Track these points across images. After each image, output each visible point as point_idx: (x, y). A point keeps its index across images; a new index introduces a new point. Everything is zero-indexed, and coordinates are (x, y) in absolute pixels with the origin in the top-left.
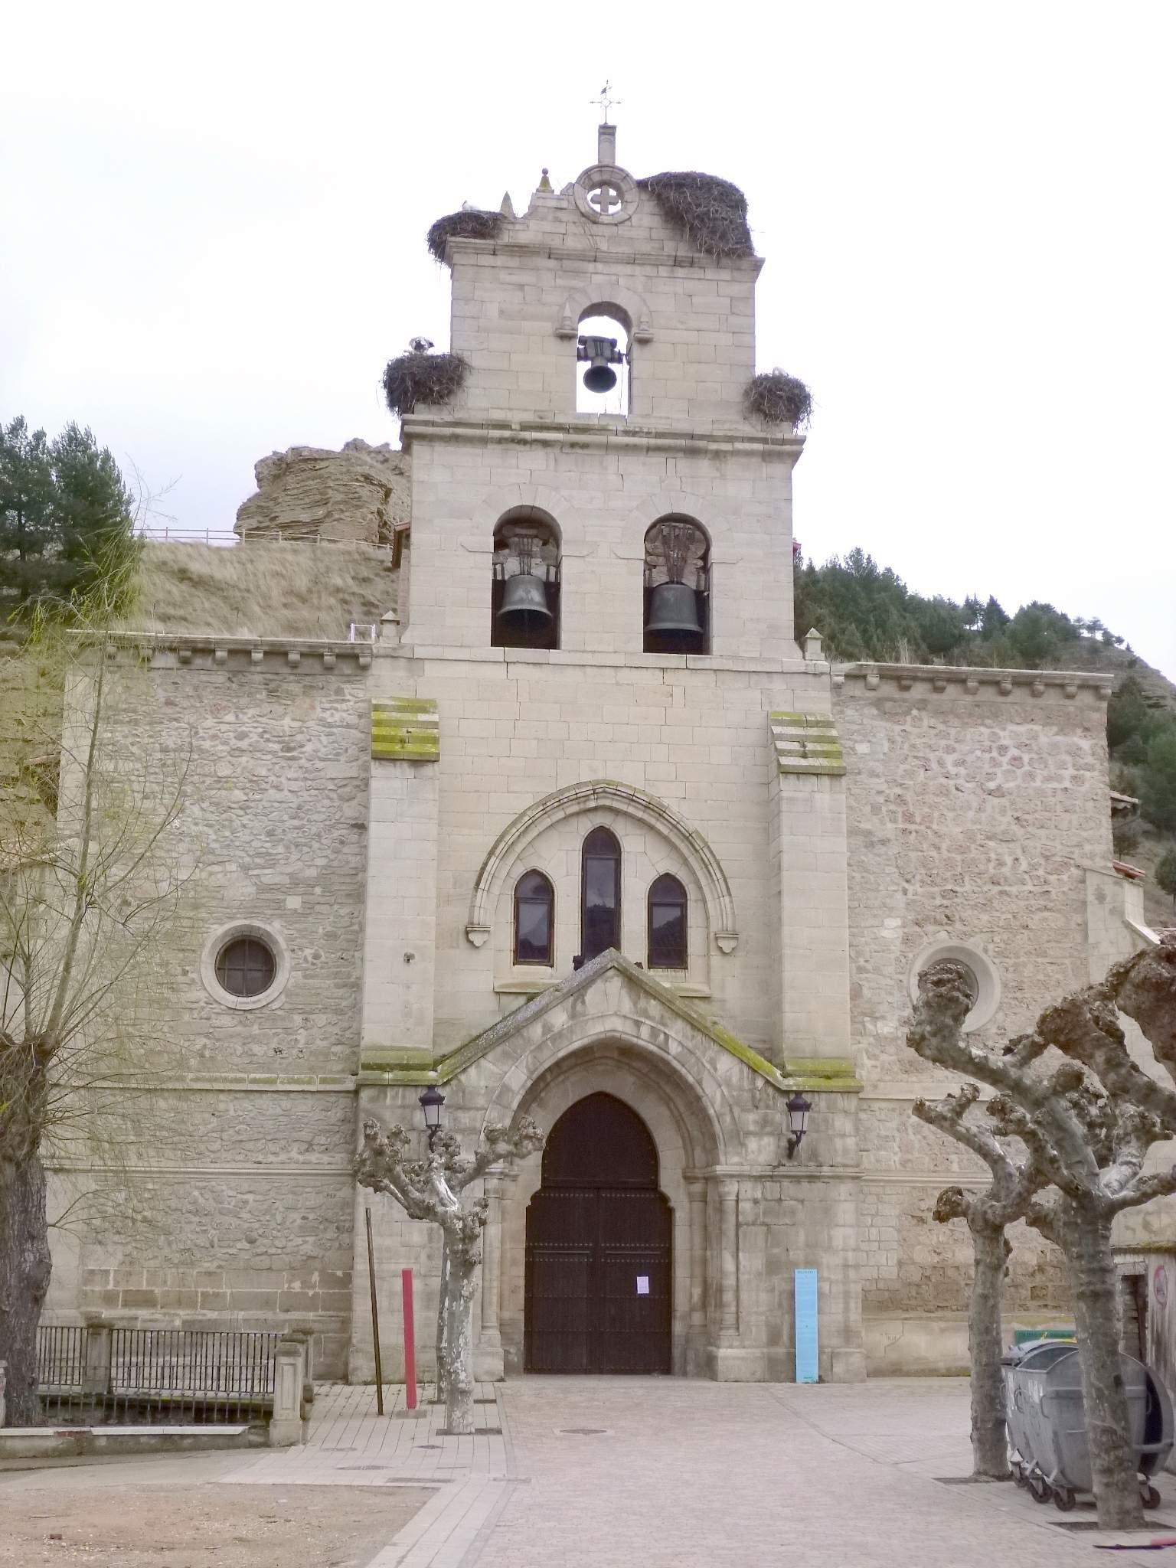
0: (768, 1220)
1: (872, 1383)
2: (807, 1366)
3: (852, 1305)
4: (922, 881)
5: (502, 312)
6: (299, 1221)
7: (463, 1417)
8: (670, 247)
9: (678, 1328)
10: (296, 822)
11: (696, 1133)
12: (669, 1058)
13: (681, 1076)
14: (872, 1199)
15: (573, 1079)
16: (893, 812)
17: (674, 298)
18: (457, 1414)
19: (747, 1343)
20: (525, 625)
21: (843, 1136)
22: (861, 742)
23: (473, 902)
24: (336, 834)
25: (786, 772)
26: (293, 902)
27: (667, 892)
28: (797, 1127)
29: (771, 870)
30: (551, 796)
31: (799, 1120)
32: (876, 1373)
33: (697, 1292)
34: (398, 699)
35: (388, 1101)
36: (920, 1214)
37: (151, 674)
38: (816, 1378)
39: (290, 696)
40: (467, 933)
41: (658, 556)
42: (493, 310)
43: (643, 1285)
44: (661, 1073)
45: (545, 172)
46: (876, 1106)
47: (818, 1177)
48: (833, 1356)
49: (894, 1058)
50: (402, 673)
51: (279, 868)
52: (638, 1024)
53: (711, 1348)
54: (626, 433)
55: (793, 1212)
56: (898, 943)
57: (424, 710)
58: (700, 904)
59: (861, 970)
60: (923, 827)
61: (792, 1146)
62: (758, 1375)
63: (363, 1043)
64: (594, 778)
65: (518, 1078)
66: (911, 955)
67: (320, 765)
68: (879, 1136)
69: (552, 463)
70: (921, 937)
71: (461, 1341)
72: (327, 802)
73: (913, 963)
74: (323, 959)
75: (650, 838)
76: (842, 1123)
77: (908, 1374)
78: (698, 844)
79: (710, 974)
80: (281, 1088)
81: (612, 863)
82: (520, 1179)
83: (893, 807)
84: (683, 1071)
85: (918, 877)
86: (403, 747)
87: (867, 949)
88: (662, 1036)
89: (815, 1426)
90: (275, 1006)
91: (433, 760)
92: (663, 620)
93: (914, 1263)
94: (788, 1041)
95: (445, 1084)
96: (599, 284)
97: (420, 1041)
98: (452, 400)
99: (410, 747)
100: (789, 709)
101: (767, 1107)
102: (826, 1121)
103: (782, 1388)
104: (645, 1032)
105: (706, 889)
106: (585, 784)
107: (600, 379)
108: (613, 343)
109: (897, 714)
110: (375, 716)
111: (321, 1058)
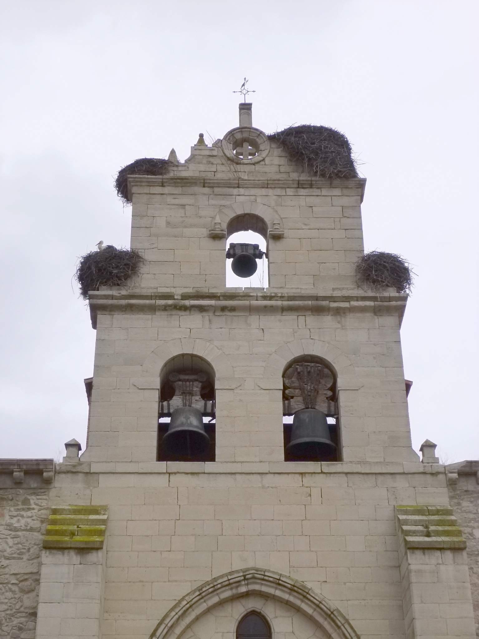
5: (168, 223)
8: (295, 176)
17: (299, 209)
24: (16, 622)
25: (413, 548)
30: (207, 583)
41: (295, 388)
42: (161, 222)
45: (201, 136)
64: (243, 566)
69: (207, 322)
72: (9, 595)
78: (340, 621)
91: (98, 548)
96: (242, 203)
98: (129, 282)
106: (237, 571)
108: (256, 247)
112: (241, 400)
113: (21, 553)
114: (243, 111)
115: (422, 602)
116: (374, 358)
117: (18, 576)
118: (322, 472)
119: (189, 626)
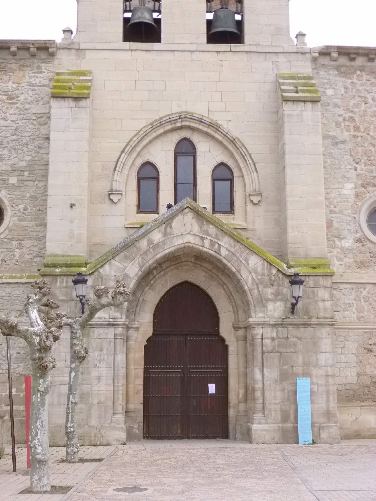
0: (280, 350)
1: (345, 444)
2: (305, 435)
3: (331, 398)
4: (365, 163)
6: (15, 355)
7: (40, 480)
9: (232, 412)
10: (15, 137)
11: (239, 302)
12: (221, 258)
13: (229, 269)
14: (342, 338)
15: (170, 274)
16: (348, 126)
18: (36, 477)
19: (269, 421)
21: (324, 301)
22: (329, 88)
23: (113, 178)
24: (36, 143)
26: (13, 180)
27: (223, 175)
28: (296, 294)
29: (279, 156)
30: (156, 121)
31: (298, 290)
32: (346, 437)
33: (242, 392)
34: (69, 70)
35: (58, 284)
36: (369, 347)
38: (311, 441)
39: (13, 71)
43: (212, 389)
44: (218, 269)
46: (342, 286)
47: (310, 325)
48: (320, 428)
49: (352, 260)
51: (4, 162)
52: (203, 239)
53: (250, 424)
55: (295, 345)
56: (353, 196)
58: (241, 179)
59: (332, 212)
60: (365, 134)
61: (293, 306)
62: (276, 440)
63: (47, 253)
65: (133, 271)
66: (360, 204)
67: (28, 106)
68: (344, 303)
70: (366, 193)
71: (38, 424)
72: (31, 126)
73: (361, 208)
74: (29, 210)
75: (212, 144)
76: (323, 294)
77: (364, 438)
78: (239, 144)
79: (249, 217)
80: (5, 281)
81: (192, 158)
82: (141, 329)
83: (347, 123)
84: (229, 265)
85: (363, 161)
87: (335, 200)
88: (217, 246)
89: (305, 482)
92: (217, 28)
93: (366, 374)
94: (291, 248)
95: (90, 274)
97: (80, 251)
99: (73, 91)
101: (279, 285)
102: (313, 292)
103: (288, 448)
104: (207, 243)
105: (243, 170)
106: (175, 113)
109: (348, 73)
111: (28, 265)
117: (37, 115)
119: (145, 147)
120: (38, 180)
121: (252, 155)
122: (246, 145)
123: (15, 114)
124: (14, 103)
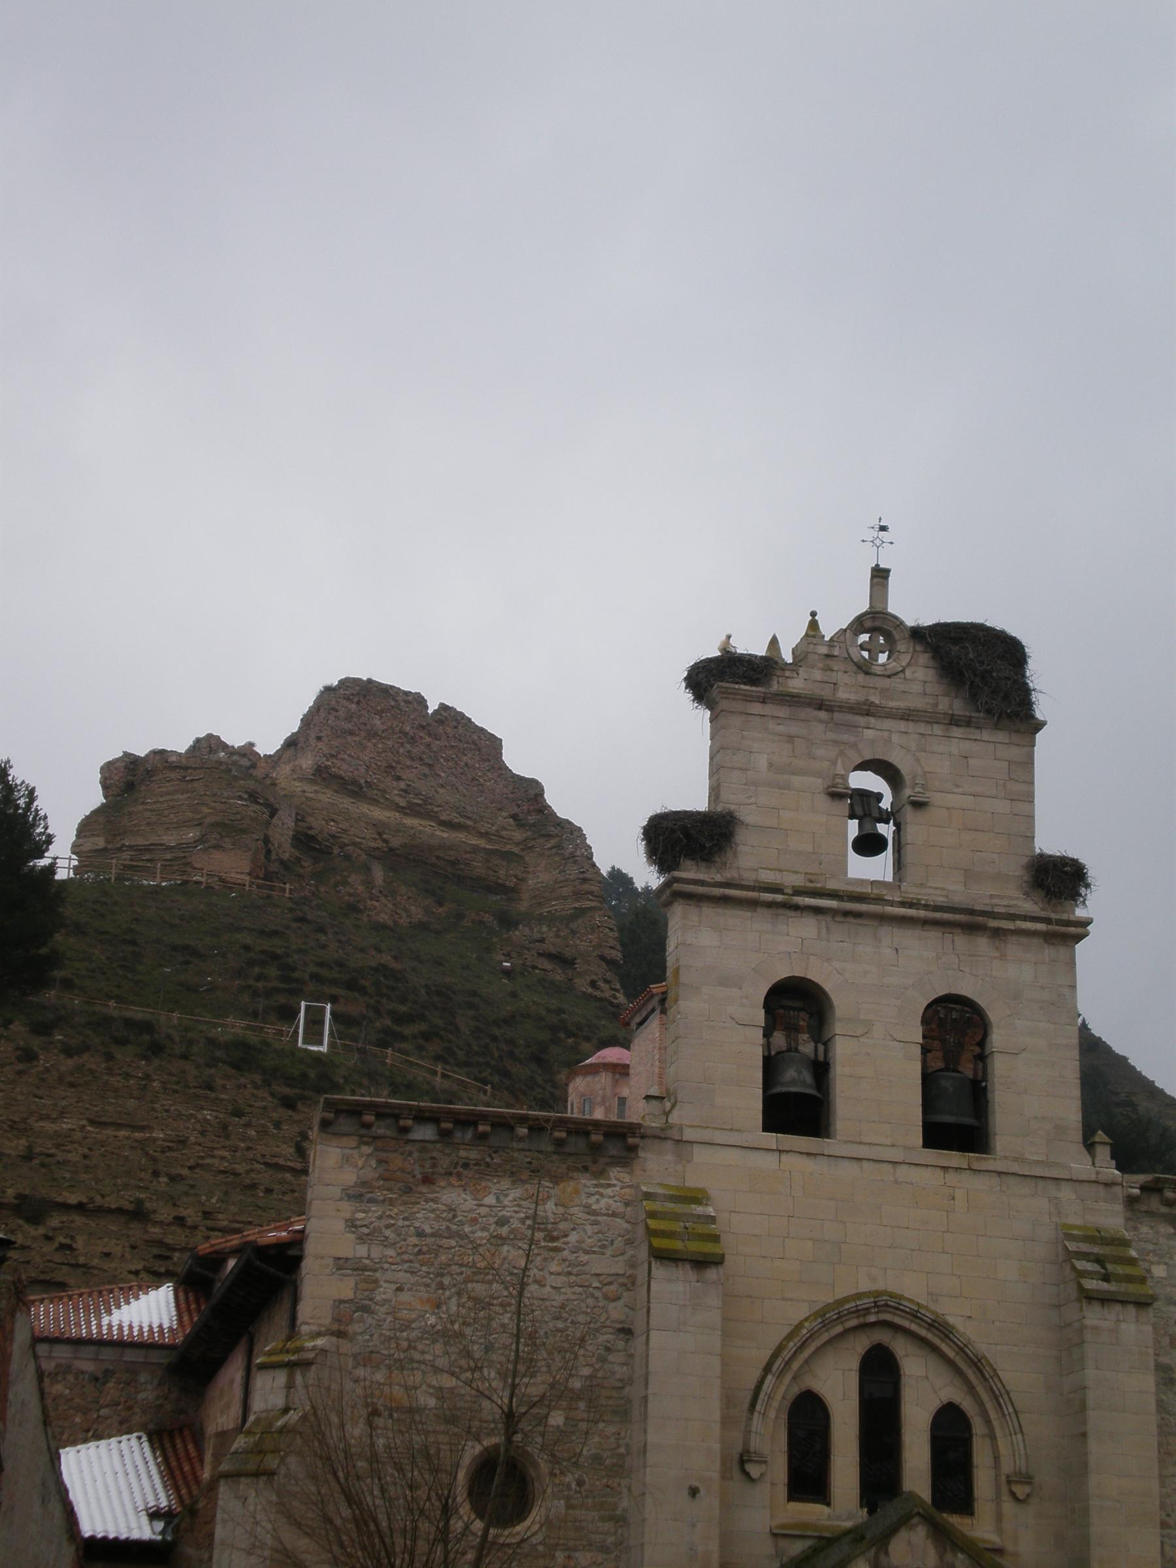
5: (770, 765)
8: (944, 704)
17: (946, 759)
20: (798, 1109)
22: (1158, 1263)
24: (602, 1338)
27: (952, 1433)
29: (1074, 1407)
37: (408, 1148)
40: (742, 1462)
42: (762, 761)
45: (813, 614)
50: (669, 1157)
54: (903, 904)
57: (697, 1201)
58: (988, 1441)
67: (584, 1258)
72: (590, 1301)
78: (987, 1372)
86: (688, 1246)
90: (534, 1540)
91: (716, 1261)
100: (1079, 1222)
105: (995, 1423)
107: (869, 845)
110: (648, 1205)
112: (868, 1054)
113: (604, 1247)
114: (876, 580)
115: (1097, 1368)
116: (1041, 1008)
117: (601, 1278)
118: (970, 1169)
119: (806, 1362)
120: (604, 1421)
121: (1012, 1394)
122: (1000, 1373)
123: (559, 1274)
124: (556, 1250)
